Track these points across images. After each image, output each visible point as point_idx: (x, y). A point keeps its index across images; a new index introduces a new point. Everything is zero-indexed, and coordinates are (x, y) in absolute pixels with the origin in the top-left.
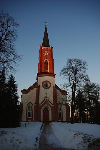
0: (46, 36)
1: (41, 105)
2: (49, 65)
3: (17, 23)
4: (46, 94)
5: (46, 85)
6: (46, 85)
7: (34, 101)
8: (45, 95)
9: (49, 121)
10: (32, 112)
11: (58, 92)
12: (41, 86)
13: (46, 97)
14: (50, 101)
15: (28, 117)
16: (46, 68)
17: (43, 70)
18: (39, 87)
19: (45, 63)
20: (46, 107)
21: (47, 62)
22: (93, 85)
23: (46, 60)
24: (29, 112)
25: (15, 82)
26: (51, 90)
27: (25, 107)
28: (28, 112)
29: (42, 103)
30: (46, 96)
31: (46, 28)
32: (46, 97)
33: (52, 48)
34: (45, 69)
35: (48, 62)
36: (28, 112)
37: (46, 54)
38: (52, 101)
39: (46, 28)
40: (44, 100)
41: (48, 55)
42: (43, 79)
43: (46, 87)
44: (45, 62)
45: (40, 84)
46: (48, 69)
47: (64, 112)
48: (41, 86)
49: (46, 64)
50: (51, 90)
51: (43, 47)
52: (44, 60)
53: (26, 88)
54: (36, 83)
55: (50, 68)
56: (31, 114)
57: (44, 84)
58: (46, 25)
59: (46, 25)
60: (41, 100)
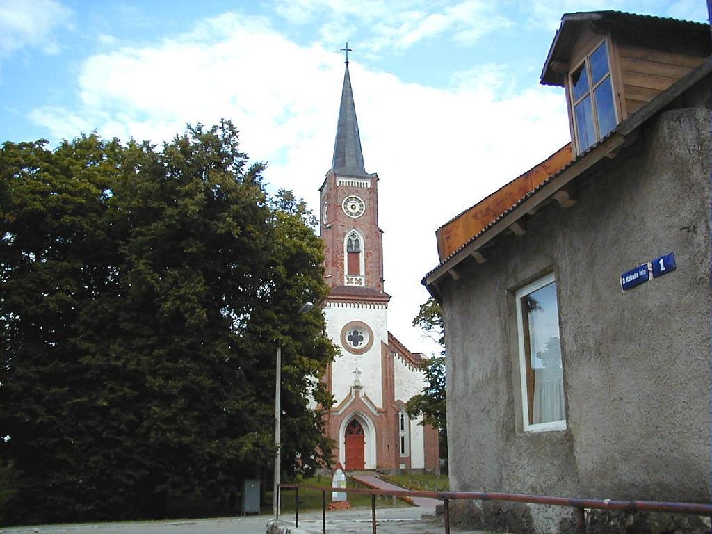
0: (349, 102)
2: (367, 255)
4: (357, 372)
8: (354, 377)
9: (366, 467)
11: (398, 362)
13: (358, 388)
16: (354, 270)
17: (342, 274)
19: (350, 246)
25: (333, 396)
26: (372, 360)
30: (355, 382)
31: (347, 77)
33: (375, 178)
35: (362, 242)
37: (353, 207)
38: (379, 403)
39: (347, 77)
41: (359, 213)
46: (362, 272)
47: (418, 434)
50: (375, 354)
51: (339, 180)
55: (369, 268)
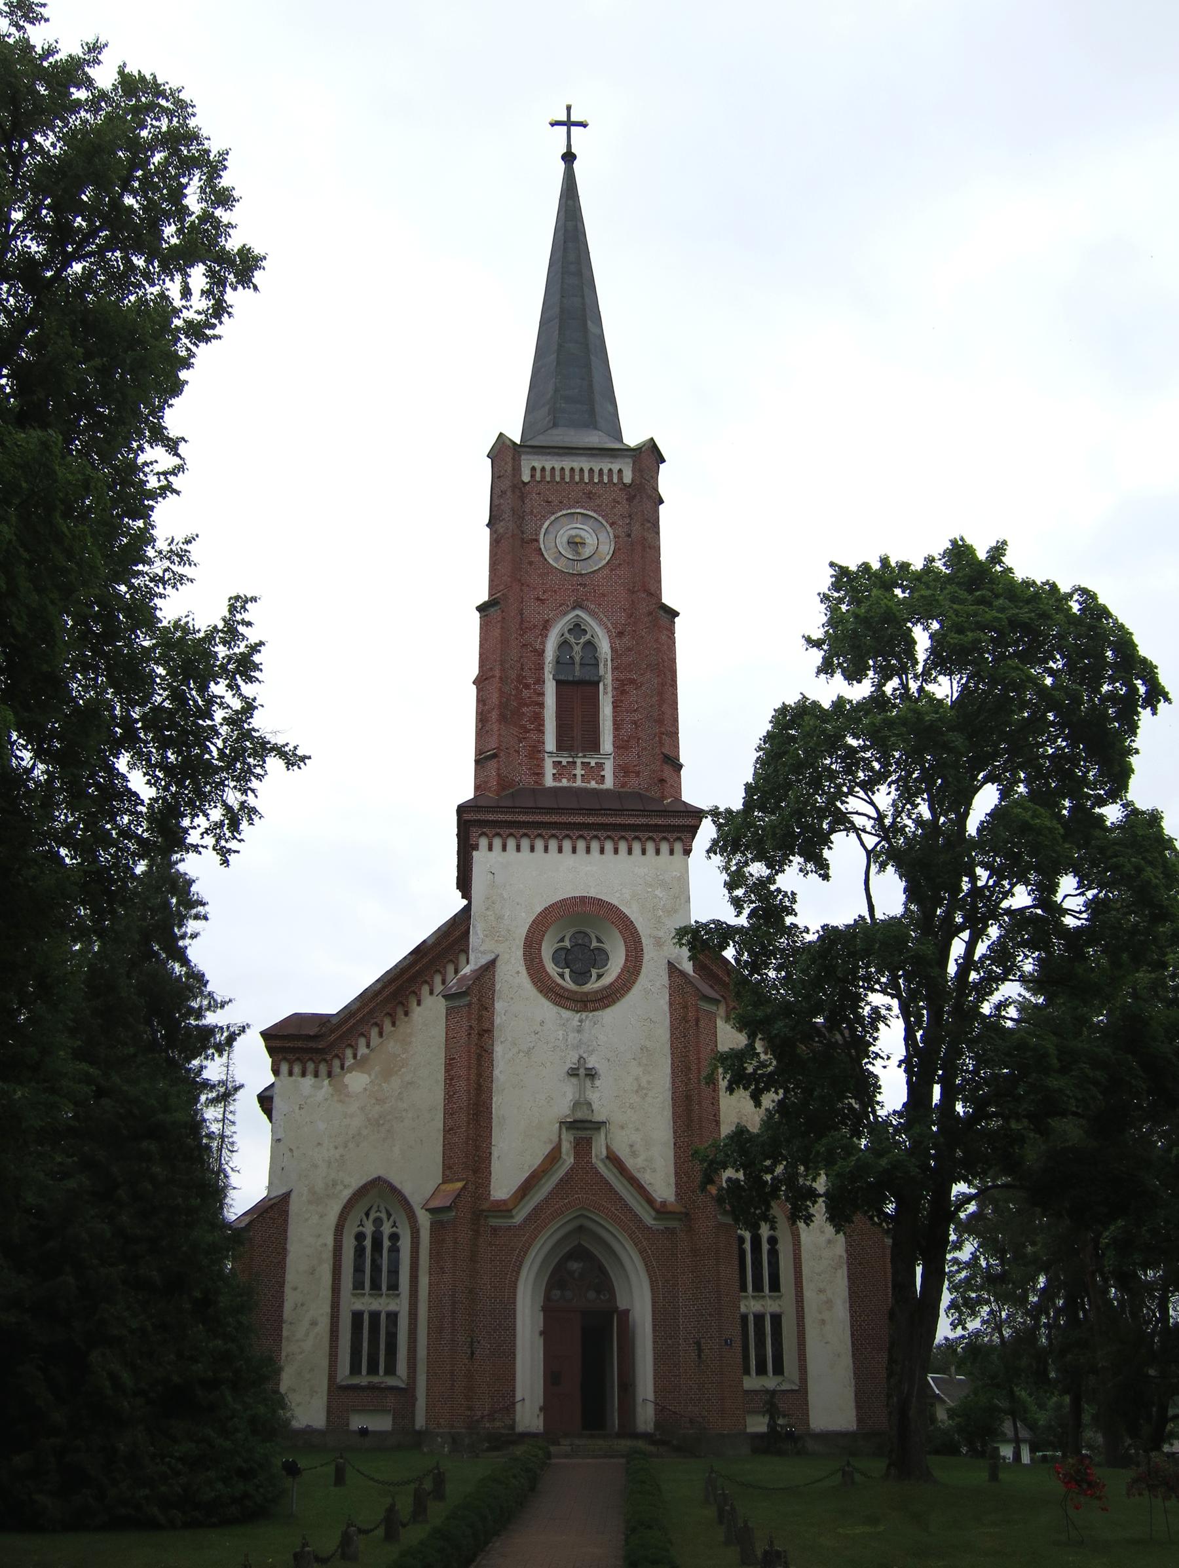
1: (519, 1217)
2: (621, 690)
3: (78, 51)
4: (582, 1073)
5: (582, 957)
6: (580, 951)
7: (420, 1176)
10: (401, 1305)
12: (513, 976)
13: (582, 1128)
14: (629, 1163)
15: (355, 1369)
16: (578, 733)
18: (474, 1008)
20: (581, 1228)
21: (590, 646)
22: (193, 137)
23: (577, 629)
24: (367, 1303)
27: (310, 1243)
28: (352, 1303)
29: (525, 1189)
30: (576, 1105)
32: (582, 1128)
34: (560, 746)
35: (604, 647)
36: (358, 1306)
40: (554, 1157)
42: (541, 875)
43: (581, 976)
44: (564, 645)
45: (499, 943)
46: (607, 744)
48: (513, 976)
49: (578, 692)
52: (546, 626)
53: (330, 1000)
54: (451, 939)
56: (392, 1337)
57: (547, 951)
58: (569, 157)
59: (569, 157)
60: (514, 1156)
